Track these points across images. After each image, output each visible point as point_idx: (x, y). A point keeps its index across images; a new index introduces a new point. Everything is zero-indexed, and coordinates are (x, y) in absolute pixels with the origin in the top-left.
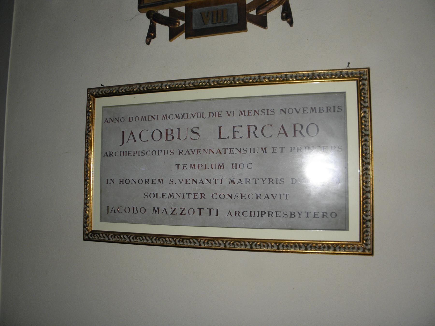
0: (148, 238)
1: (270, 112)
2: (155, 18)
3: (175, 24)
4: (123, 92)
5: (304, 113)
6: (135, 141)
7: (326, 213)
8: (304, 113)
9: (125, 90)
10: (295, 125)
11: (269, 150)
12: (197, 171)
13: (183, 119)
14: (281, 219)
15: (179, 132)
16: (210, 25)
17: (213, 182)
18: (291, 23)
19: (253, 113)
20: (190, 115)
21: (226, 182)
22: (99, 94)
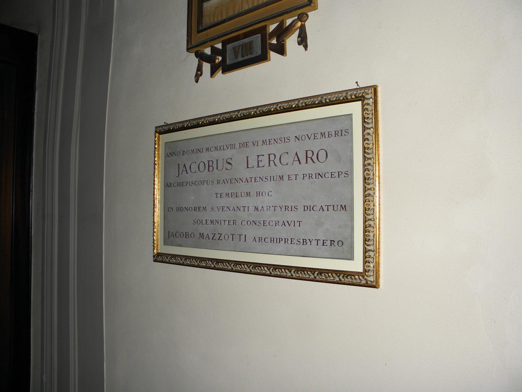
0: (334, 275)
1: (286, 140)
2: (202, 57)
3: (215, 61)
4: (302, 106)
5: (315, 139)
6: (187, 173)
7: (334, 241)
8: (315, 139)
9: (305, 103)
10: (307, 151)
11: (286, 178)
12: (230, 199)
13: (220, 151)
14: (295, 246)
15: (217, 163)
16: (240, 59)
17: (242, 209)
18: (306, 47)
19: (272, 141)
20: (225, 147)
21: (252, 209)
22: (277, 110)
